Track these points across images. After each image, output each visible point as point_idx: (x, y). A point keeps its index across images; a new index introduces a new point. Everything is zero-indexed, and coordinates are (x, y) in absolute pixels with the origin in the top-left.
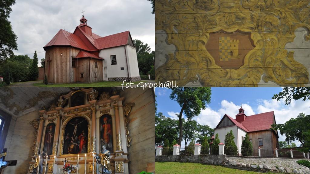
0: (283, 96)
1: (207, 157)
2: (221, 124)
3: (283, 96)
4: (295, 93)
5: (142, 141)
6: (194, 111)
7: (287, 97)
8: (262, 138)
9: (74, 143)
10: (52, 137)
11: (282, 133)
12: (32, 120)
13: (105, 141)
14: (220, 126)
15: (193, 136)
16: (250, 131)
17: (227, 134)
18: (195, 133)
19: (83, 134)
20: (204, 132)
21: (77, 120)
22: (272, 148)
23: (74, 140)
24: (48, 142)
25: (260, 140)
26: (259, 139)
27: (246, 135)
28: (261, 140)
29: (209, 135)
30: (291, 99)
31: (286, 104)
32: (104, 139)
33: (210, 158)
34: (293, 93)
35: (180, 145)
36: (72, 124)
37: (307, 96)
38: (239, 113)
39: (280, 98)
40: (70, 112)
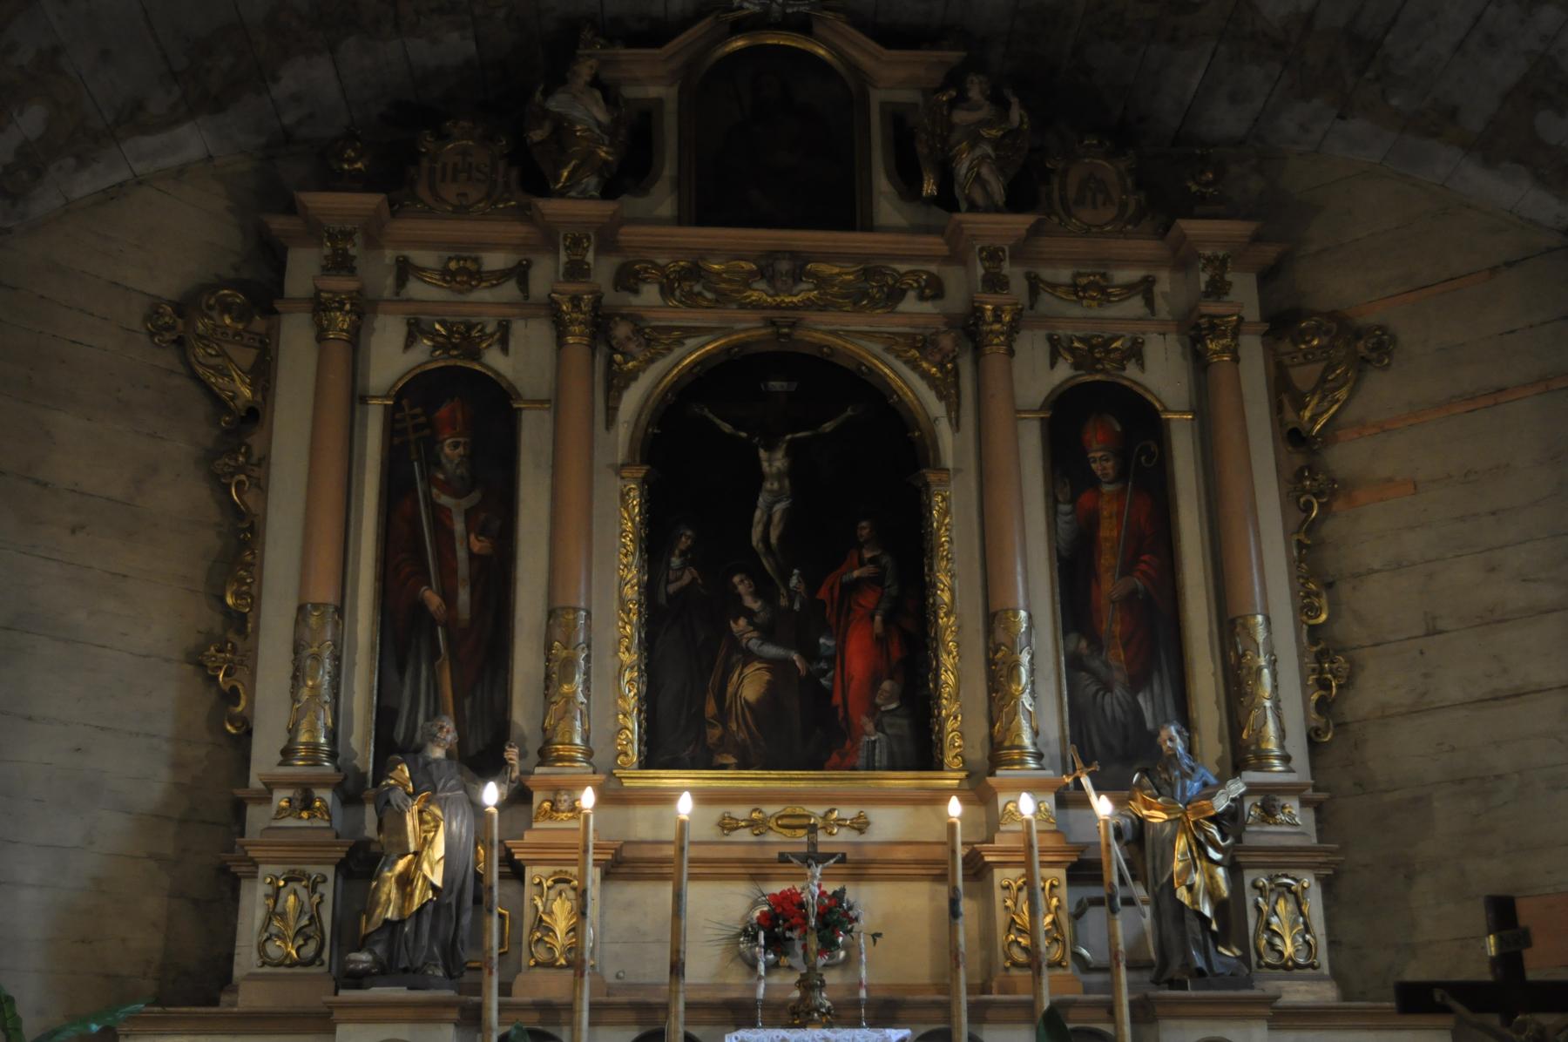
5: (1454, 706)
9: (771, 651)
10: (478, 545)
12: (167, 285)
13: (1107, 665)
19: (868, 555)
21: (776, 385)
23: (762, 617)
24: (433, 599)
32: (1096, 643)
36: (727, 428)
40: (695, 272)
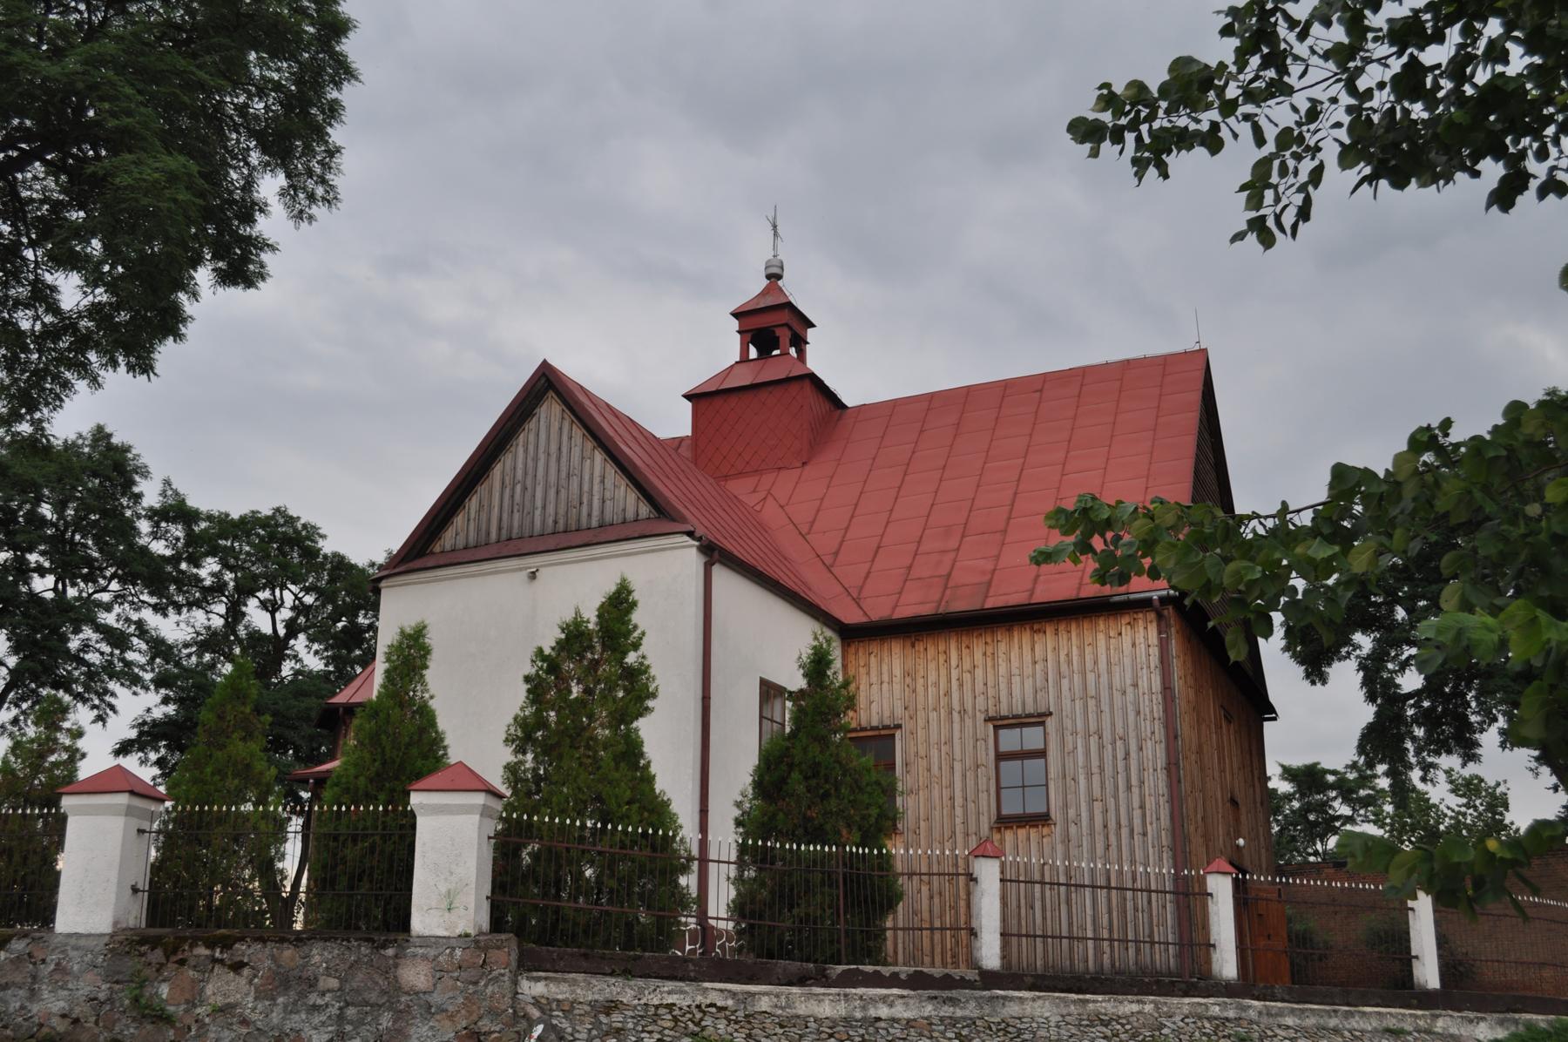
0: (1214, 115)
1: (237, 967)
2: (473, 503)
3: (1214, 115)
4: (1368, 94)
6: (95, 310)
7: (1270, 133)
8: (1038, 719)
11: (1315, 663)
14: (452, 537)
15: (78, 659)
16: (879, 610)
17: (549, 639)
18: (109, 619)
20: (235, 614)
22: (1181, 853)
25: (1011, 740)
26: (1000, 723)
27: (817, 666)
28: (1031, 738)
29: (308, 656)
30: (1317, 176)
31: (1258, 225)
34: (1351, 89)
37: (1542, 155)
38: (744, 359)
39: (1184, 139)
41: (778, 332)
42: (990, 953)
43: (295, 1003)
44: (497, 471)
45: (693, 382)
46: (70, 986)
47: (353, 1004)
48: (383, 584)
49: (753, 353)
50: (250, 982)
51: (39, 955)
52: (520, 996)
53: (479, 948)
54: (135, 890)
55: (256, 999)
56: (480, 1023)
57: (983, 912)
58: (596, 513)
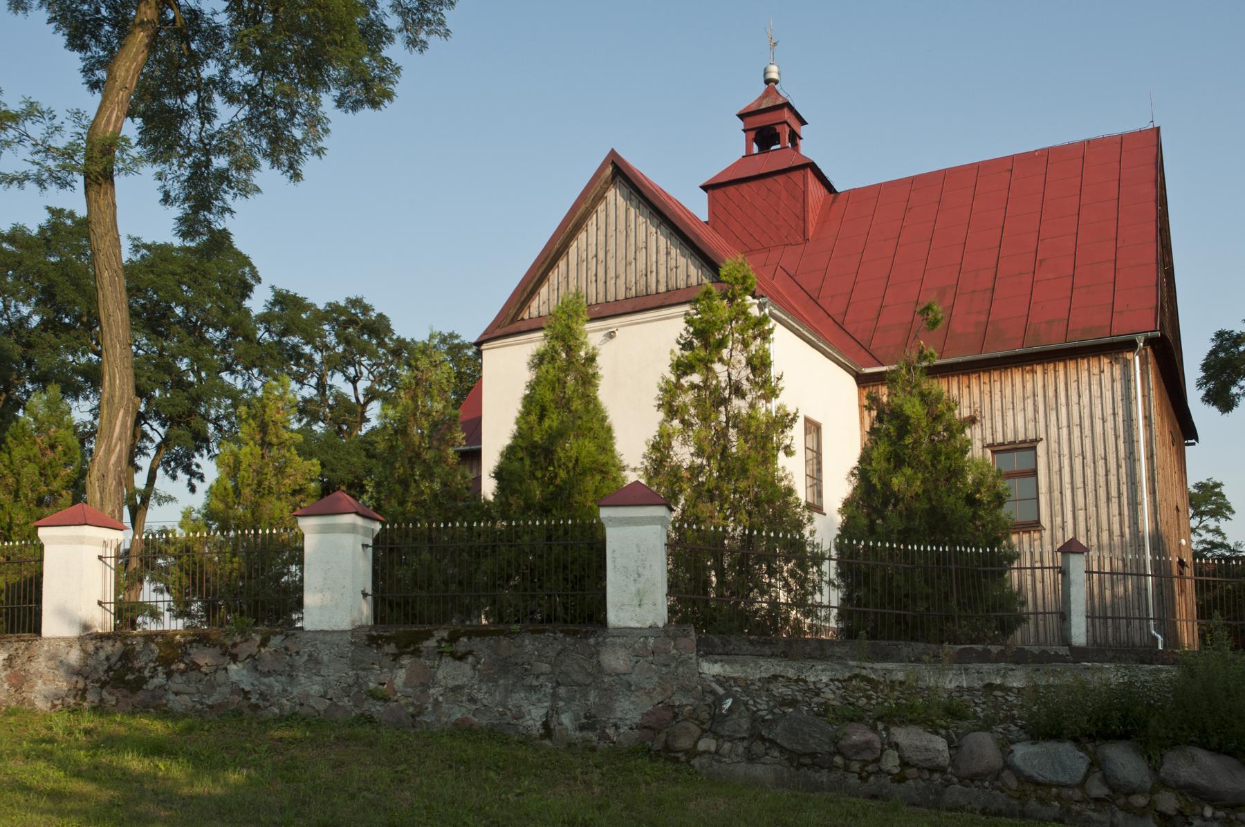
2: (554, 276)
33: (504, 667)
35: (73, 504)
38: (749, 155)
41: (779, 129)
42: (1079, 632)
43: (514, 685)
44: (573, 250)
45: (708, 176)
46: (322, 673)
47: (563, 684)
48: (484, 347)
49: (755, 149)
50: (474, 667)
51: (294, 649)
52: (703, 676)
53: (669, 636)
54: (365, 595)
55: (481, 681)
56: (674, 698)
57: (1072, 598)
58: (663, 280)
